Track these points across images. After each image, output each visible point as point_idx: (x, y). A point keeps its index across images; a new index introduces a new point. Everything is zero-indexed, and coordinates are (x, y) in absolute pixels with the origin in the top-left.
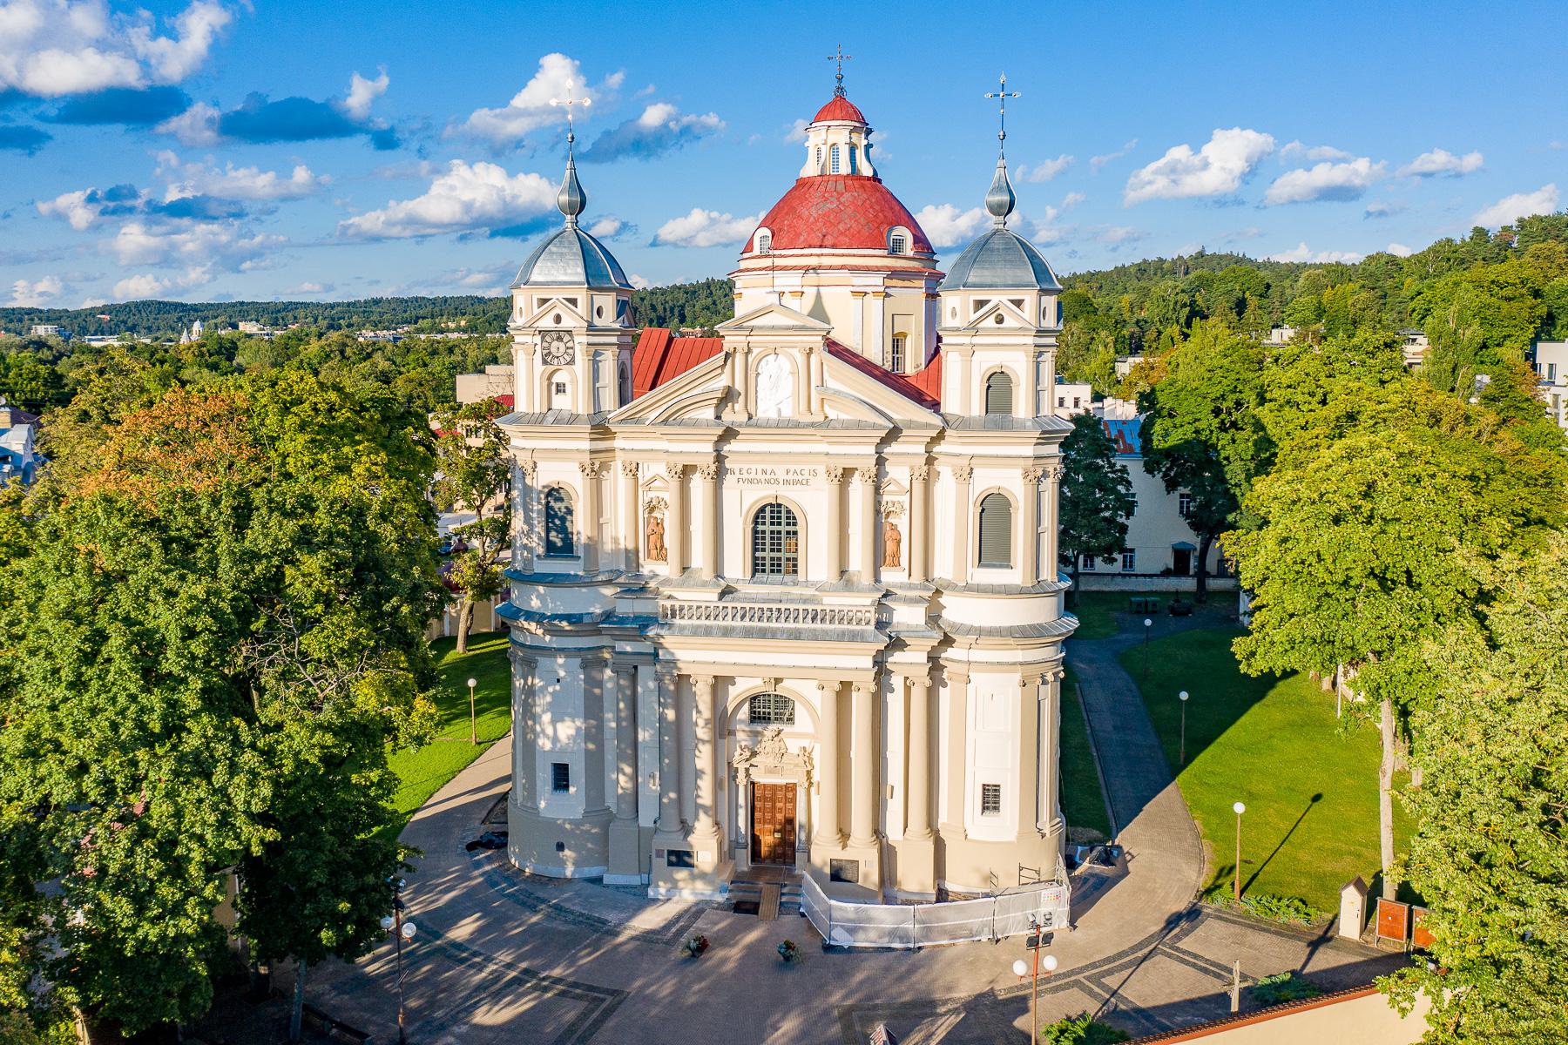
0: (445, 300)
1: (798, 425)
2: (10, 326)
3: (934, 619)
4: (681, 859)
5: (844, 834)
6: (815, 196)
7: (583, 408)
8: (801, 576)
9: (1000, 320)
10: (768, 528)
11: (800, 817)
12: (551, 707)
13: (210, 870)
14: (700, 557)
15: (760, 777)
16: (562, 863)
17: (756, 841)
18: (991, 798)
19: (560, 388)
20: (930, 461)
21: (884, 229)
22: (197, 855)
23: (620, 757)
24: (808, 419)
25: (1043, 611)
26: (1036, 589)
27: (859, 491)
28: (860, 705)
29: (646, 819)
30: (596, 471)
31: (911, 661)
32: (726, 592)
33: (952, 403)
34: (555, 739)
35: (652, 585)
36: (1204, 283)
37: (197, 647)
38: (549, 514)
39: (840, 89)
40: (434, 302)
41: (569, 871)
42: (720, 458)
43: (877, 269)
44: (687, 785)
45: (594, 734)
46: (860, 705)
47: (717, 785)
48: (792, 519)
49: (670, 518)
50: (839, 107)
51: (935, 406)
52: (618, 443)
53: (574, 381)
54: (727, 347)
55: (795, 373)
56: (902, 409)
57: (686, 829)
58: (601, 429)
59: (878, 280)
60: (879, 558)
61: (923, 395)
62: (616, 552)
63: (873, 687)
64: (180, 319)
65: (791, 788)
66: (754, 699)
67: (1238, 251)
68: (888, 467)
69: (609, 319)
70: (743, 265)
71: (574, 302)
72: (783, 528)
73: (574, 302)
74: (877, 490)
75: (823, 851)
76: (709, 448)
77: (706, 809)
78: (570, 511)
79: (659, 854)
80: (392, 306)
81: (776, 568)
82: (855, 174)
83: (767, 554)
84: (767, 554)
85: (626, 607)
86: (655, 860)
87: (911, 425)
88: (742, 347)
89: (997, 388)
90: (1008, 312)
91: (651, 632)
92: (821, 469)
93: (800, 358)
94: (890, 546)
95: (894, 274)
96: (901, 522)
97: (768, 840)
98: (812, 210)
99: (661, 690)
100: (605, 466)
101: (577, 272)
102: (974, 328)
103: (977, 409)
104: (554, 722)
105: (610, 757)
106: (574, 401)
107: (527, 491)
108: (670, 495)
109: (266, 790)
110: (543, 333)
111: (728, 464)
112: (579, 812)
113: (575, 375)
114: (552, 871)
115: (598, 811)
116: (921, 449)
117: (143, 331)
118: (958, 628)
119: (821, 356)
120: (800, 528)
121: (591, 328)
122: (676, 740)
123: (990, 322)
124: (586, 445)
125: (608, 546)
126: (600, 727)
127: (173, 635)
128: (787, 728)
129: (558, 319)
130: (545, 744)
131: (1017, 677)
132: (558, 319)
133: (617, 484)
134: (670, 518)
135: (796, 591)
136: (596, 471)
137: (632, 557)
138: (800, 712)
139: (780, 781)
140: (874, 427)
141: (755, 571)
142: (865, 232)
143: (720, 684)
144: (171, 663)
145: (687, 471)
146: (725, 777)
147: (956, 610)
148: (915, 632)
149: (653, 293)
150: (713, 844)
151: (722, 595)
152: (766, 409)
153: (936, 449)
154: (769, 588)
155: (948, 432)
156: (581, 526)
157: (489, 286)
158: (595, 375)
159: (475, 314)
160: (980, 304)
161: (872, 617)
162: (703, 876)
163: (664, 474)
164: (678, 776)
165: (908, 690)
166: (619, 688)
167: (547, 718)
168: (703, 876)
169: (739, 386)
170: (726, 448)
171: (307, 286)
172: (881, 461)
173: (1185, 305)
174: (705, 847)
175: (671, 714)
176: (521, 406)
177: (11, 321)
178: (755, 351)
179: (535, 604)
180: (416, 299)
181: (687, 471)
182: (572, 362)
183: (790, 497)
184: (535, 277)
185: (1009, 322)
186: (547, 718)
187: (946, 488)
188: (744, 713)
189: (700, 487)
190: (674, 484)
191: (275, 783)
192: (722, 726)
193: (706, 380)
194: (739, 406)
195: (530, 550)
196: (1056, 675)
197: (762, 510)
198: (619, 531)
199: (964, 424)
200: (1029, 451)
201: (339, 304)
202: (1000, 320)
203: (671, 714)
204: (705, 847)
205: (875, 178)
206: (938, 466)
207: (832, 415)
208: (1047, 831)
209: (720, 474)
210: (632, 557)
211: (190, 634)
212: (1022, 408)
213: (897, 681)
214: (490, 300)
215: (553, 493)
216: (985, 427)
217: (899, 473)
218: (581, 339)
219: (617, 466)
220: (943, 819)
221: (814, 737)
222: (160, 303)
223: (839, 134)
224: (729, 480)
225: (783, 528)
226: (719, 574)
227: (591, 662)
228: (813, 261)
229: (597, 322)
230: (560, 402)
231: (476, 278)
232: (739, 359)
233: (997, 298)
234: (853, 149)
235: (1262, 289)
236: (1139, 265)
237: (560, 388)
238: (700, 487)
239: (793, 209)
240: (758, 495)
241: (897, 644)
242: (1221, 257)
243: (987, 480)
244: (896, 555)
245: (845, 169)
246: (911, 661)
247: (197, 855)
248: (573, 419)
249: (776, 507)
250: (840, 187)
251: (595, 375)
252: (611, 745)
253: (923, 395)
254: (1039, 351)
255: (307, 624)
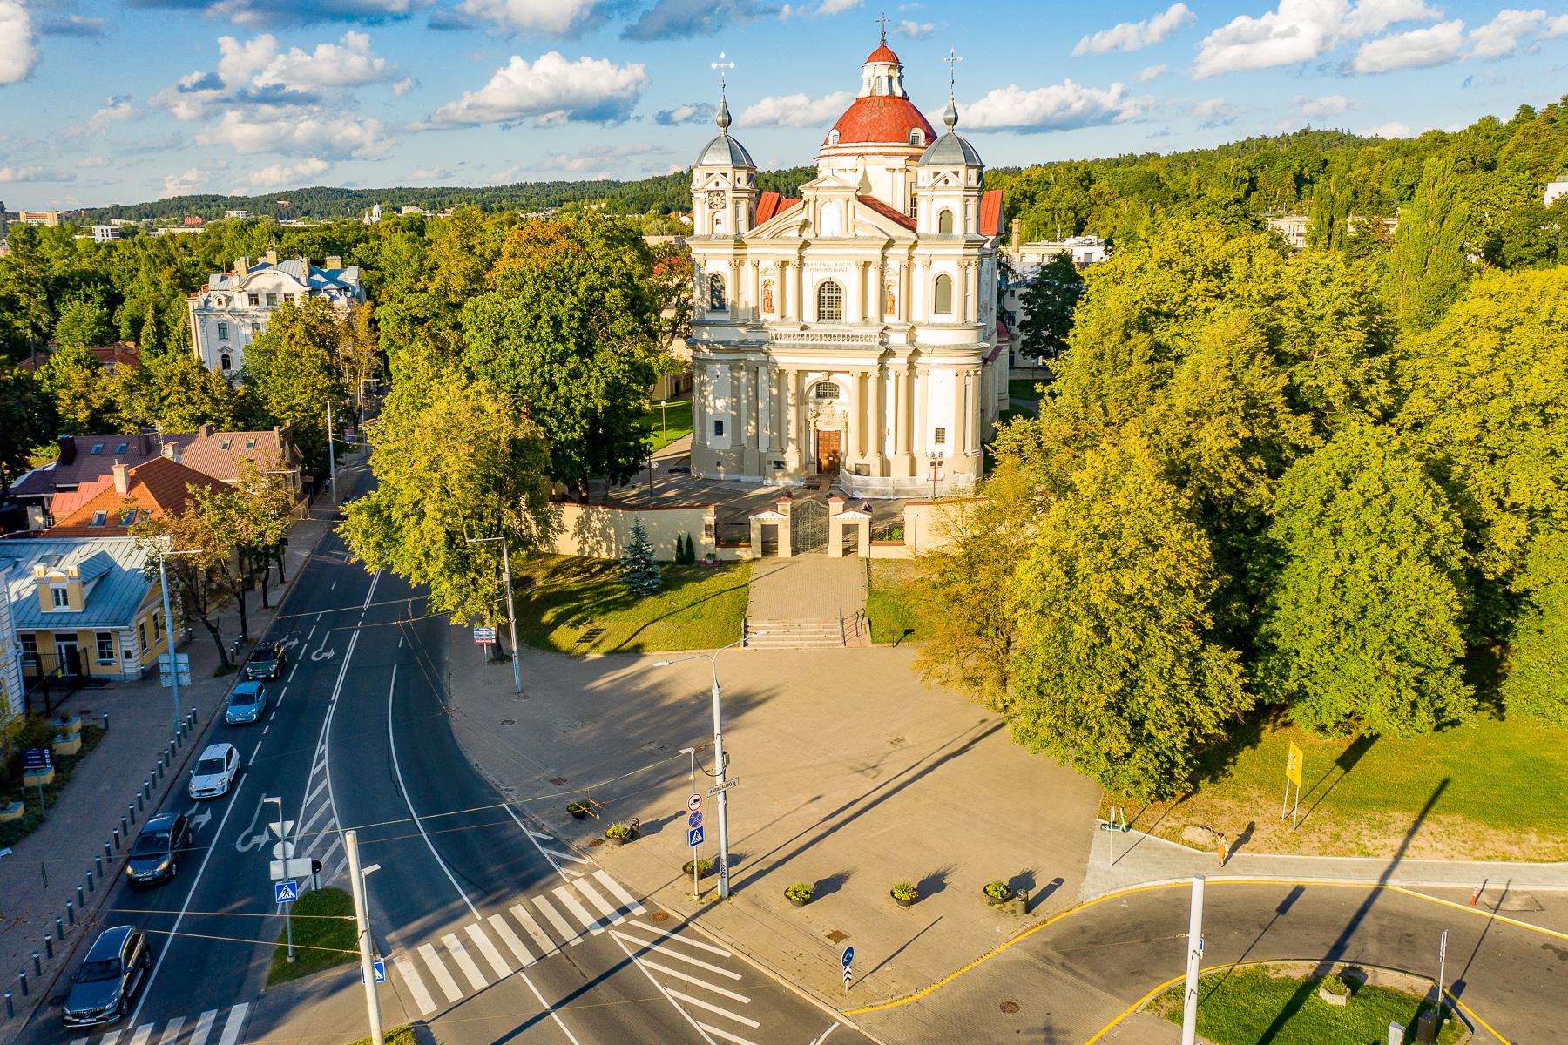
0: (584, 184)
1: (841, 239)
2: (201, 212)
3: (911, 342)
4: (780, 465)
5: (863, 454)
6: (866, 109)
7: (730, 232)
8: (843, 320)
9: (947, 182)
10: (826, 295)
11: (843, 449)
12: (713, 392)
13: (582, 416)
14: (791, 312)
15: (821, 427)
16: (719, 472)
17: (819, 462)
18: (940, 435)
19: (718, 221)
20: (910, 258)
21: (907, 129)
22: (578, 408)
23: (750, 416)
24: (845, 236)
25: (968, 338)
26: (965, 326)
27: (873, 274)
28: (872, 384)
29: (763, 449)
30: (737, 265)
31: (898, 363)
32: (804, 328)
33: (921, 229)
34: (715, 408)
35: (766, 325)
36: (1268, 161)
37: (575, 324)
38: (713, 290)
39: (883, 40)
40: (574, 186)
41: (722, 476)
42: (801, 258)
43: (902, 155)
44: (783, 430)
45: (737, 407)
46: (872, 384)
47: (799, 430)
48: (838, 290)
49: (775, 290)
50: (884, 53)
51: (914, 230)
52: (748, 251)
53: (725, 218)
54: (805, 197)
55: (841, 212)
56: (896, 230)
57: (783, 451)
58: (740, 243)
59: (901, 161)
60: (883, 309)
61: (908, 222)
62: (746, 310)
63: (878, 375)
64: (348, 204)
65: (837, 433)
66: (819, 385)
67: (520, 181)
68: (888, 261)
69: (743, 184)
70: (824, 152)
71: (725, 175)
72: (834, 295)
73: (725, 175)
74: (882, 273)
75: (851, 460)
76: (795, 252)
77: (792, 440)
78: (723, 288)
79: (769, 463)
80: (537, 190)
81: (830, 316)
82: (891, 95)
83: (826, 309)
84: (826, 309)
85: (754, 337)
86: (767, 466)
87: (899, 238)
88: (813, 198)
89: (945, 218)
90: (951, 177)
91: (765, 348)
92: (853, 263)
93: (843, 204)
94: (889, 304)
95: (913, 157)
96: (895, 290)
97: (825, 462)
98: (864, 119)
99: (770, 379)
100: (741, 263)
101: (727, 159)
102: (933, 187)
103: (935, 230)
104: (714, 399)
105: (744, 418)
106: (726, 228)
107: (701, 276)
108: (775, 278)
109: (603, 385)
110: (710, 192)
111: (805, 261)
112: (728, 447)
113: (726, 214)
114: (714, 476)
115: (738, 447)
116: (905, 252)
117: (317, 216)
118: (922, 346)
119: (854, 202)
120: (843, 295)
121: (734, 189)
122: (778, 404)
123: (942, 183)
124: (732, 251)
125: (743, 306)
126: (739, 399)
127: (565, 317)
128: (835, 401)
129: (717, 184)
130: (710, 411)
131: (953, 372)
132: (717, 184)
133: (748, 272)
134: (775, 290)
135: (840, 327)
136: (737, 265)
137: (755, 310)
138: (842, 391)
139: (833, 429)
140: (880, 239)
141: (819, 318)
142: (895, 132)
143: (801, 374)
144: (565, 331)
145: (784, 264)
146: (803, 426)
147: (923, 337)
148: (900, 346)
149: (776, 175)
150: (796, 457)
151: (802, 329)
152: (825, 232)
153: (914, 252)
154: (827, 327)
155: (919, 242)
156: (729, 295)
157: (597, 169)
158: (737, 214)
159: (613, 197)
160: (936, 174)
161: (878, 340)
162: (789, 475)
163: (773, 266)
164: (779, 424)
165: (897, 378)
166: (749, 380)
167: (711, 397)
168: (789, 475)
169: (811, 219)
170: (805, 252)
171: (421, 174)
172: (884, 258)
173: (1243, 181)
174: (792, 460)
175: (775, 391)
176: (697, 232)
177: (201, 208)
178: (820, 200)
179: (705, 336)
180: (557, 183)
181: (784, 264)
182: (724, 207)
183: (838, 278)
184: (705, 162)
185: (951, 183)
186: (711, 397)
187: (919, 273)
188: (813, 392)
189: (791, 272)
190: (777, 271)
191: (607, 382)
192: (801, 399)
193: (793, 215)
194: (811, 230)
195: (703, 308)
196: (976, 372)
197: (823, 285)
198: (749, 298)
199: (928, 237)
200: (961, 251)
201: (487, 189)
202: (947, 182)
203: (775, 391)
204: (792, 460)
205: (905, 98)
206: (915, 261)
207: (859, 233)
208: (970, 454)
209: (801, 266)
210: (755, 310)
211: (571, 317)
212: (957, 229)
213: (891, 374)
214: (625, 184)
215: (715, 278)
216: (938, 238)
217: (893, 265)
218: (729, 195)
219: (748, 263)
220: (916, 448)
221: (849, 404)
222: (328, 189)
223: (881, 69)
224: (805, 269)
225: (834, 295)
226: (800, 318)
227: (734, 366)
228: (862, 150)
229: (738, 185)
230: (718, 229)
231: (577, 164)
232: (811, 204)
233: (946, 171)
234: (890, 79)
235: (1319, 165)
236: (1243, 143)
237: (718, 221)
238: (791, 272)
239: (852, 118)
240: (822, 277)
241: (889, 353)
242: (1324, 134)
243: (939, 267)
244: (892, 308)
245: (885, 92)
246: (898, 363)
247: (578, 408)
248: (726, 237)
249: (830, 283)
250: (882, 104)
251: (737, 214)
252: (745, 412)
253: (908, 222)
254: (967, 199)
255: (612, 319)
